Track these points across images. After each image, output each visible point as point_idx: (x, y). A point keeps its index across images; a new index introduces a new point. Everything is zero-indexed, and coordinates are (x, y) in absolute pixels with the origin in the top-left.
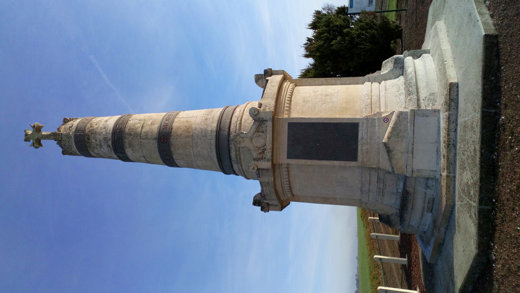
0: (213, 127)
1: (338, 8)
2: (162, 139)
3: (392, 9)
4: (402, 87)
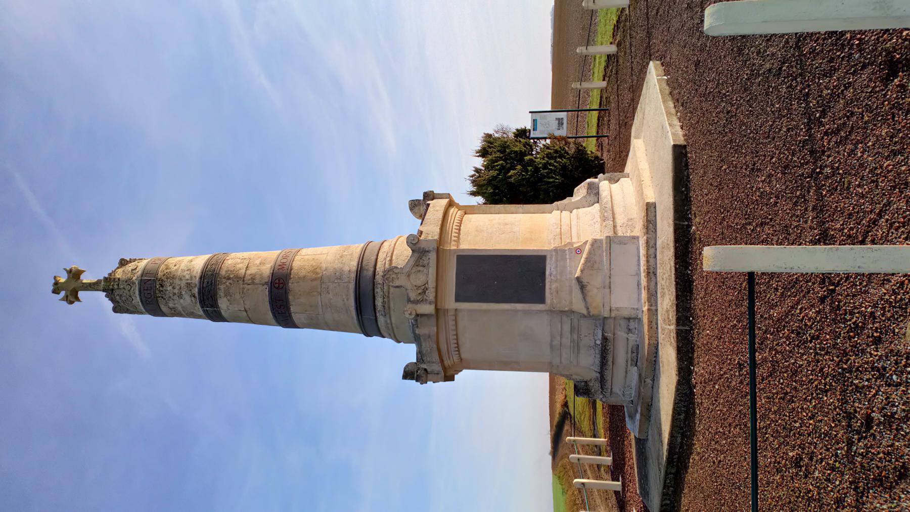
0: (351, 266)
1: (517, 130)
2: (276, 283)
3: (591, 135)
4: (598, 215)
